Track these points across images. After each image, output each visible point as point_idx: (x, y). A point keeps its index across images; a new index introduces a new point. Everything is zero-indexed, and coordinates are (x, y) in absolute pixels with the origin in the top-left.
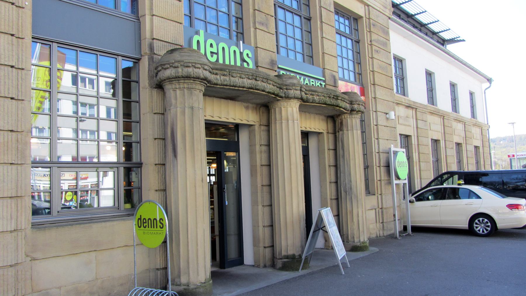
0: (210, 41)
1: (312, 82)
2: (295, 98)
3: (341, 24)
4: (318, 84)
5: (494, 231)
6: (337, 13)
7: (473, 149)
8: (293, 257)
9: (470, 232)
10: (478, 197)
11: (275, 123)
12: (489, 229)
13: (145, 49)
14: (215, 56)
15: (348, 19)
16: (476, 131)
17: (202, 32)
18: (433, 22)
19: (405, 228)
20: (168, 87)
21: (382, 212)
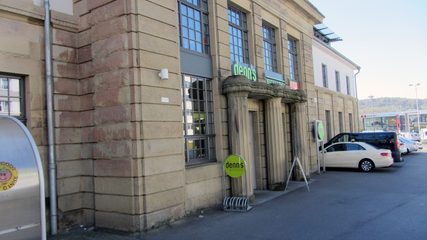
0: (240, 66)
2: (281, 97)
3: (232, 17)
5: (374, 169)
6: (229, 8)
7: (338, 114)
8: (281, 183)
9: (359, 170)
10: (364, 149)
11: (270, 111)
12: (370, 168)
13: (216, 74)
15: (239, 13)
16: (350, 103)
18: (324, 29)
19: (322, 168)
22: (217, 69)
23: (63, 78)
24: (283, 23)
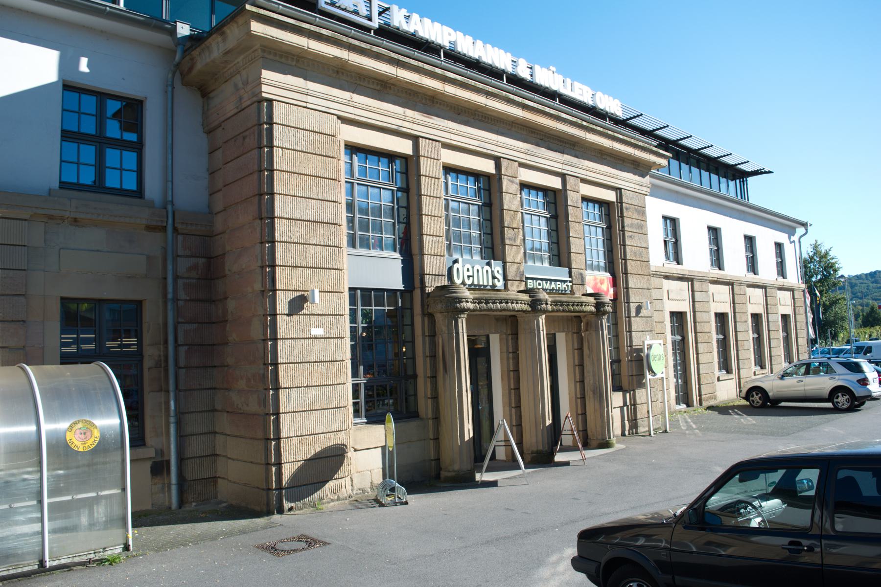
1: (559, 285)
23: (191, 300)
24: (570, 181)
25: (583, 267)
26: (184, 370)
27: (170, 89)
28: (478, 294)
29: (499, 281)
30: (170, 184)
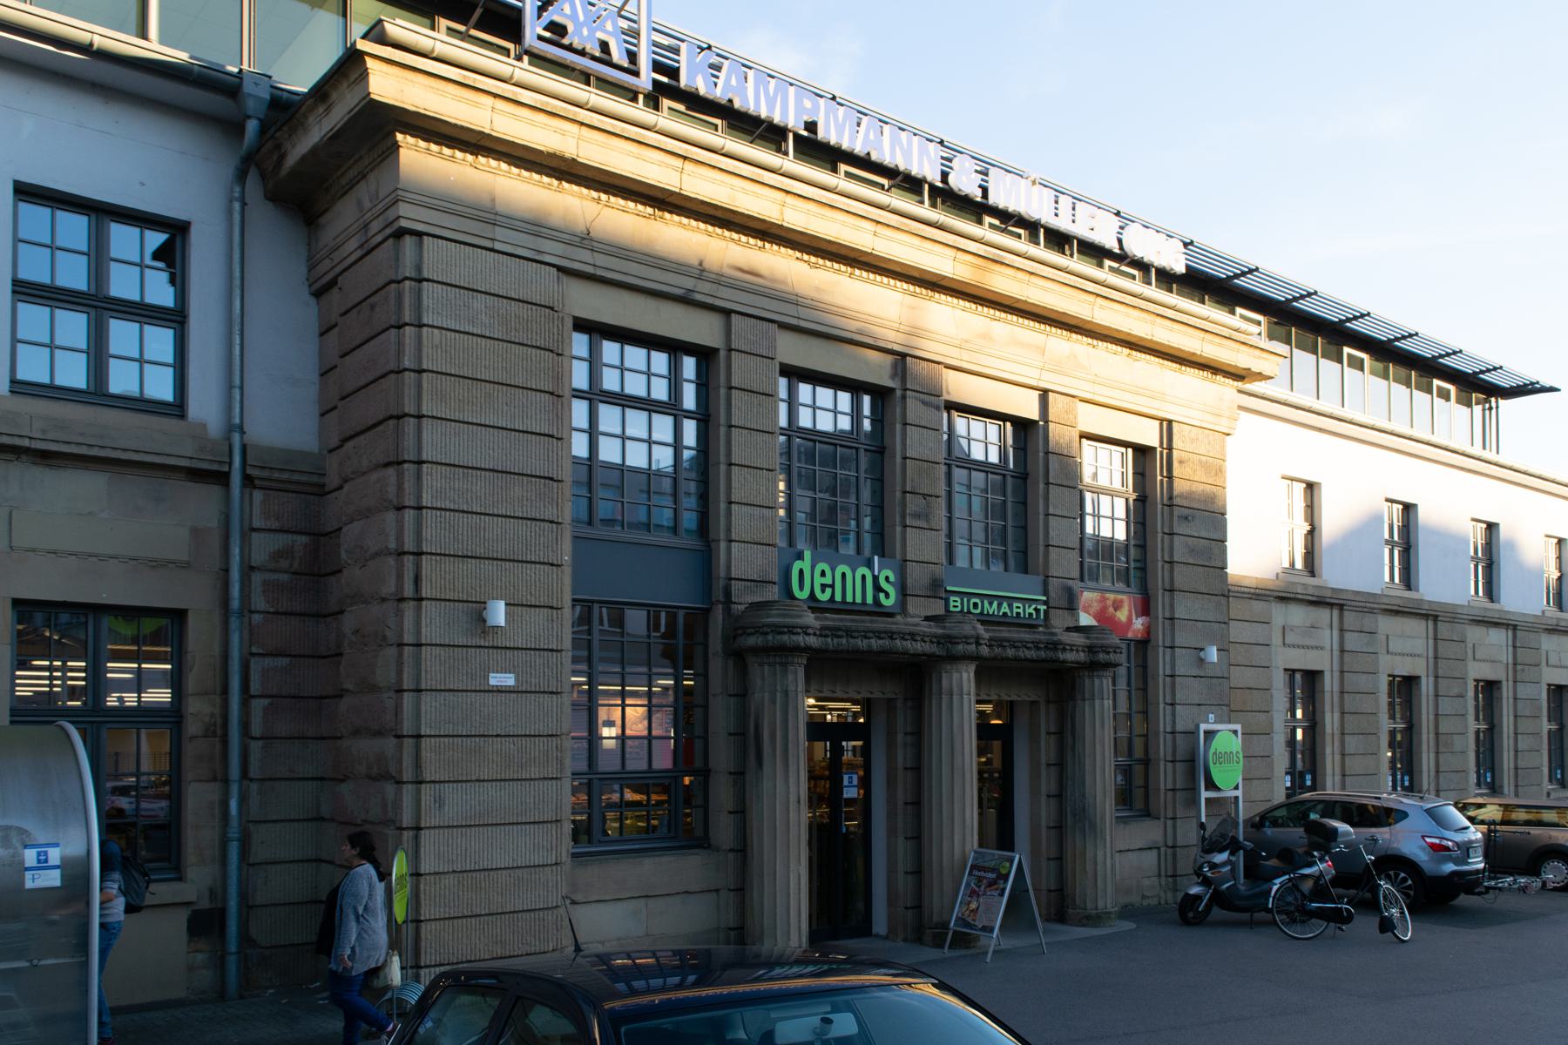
4: (1031, 610)
14: (828, 591)
17: (807, 555)
20: (751, 660)
21: (1174, 855)
22: (722, 583)
23: (277, 613)
25: (1076, 573)
26: (260, 743)
27: (237, 206)
28: (832, 620)
29: (887, 595)
30: (237, 394)
